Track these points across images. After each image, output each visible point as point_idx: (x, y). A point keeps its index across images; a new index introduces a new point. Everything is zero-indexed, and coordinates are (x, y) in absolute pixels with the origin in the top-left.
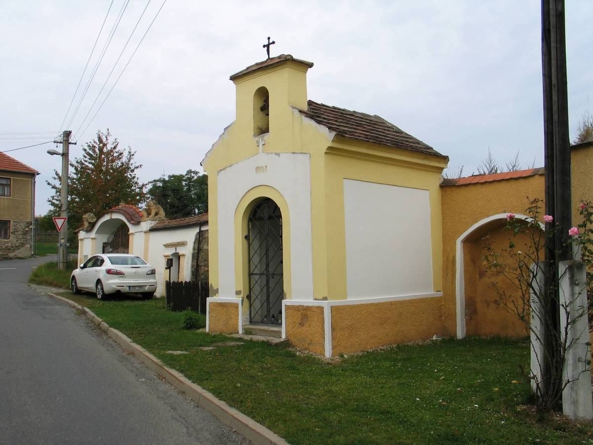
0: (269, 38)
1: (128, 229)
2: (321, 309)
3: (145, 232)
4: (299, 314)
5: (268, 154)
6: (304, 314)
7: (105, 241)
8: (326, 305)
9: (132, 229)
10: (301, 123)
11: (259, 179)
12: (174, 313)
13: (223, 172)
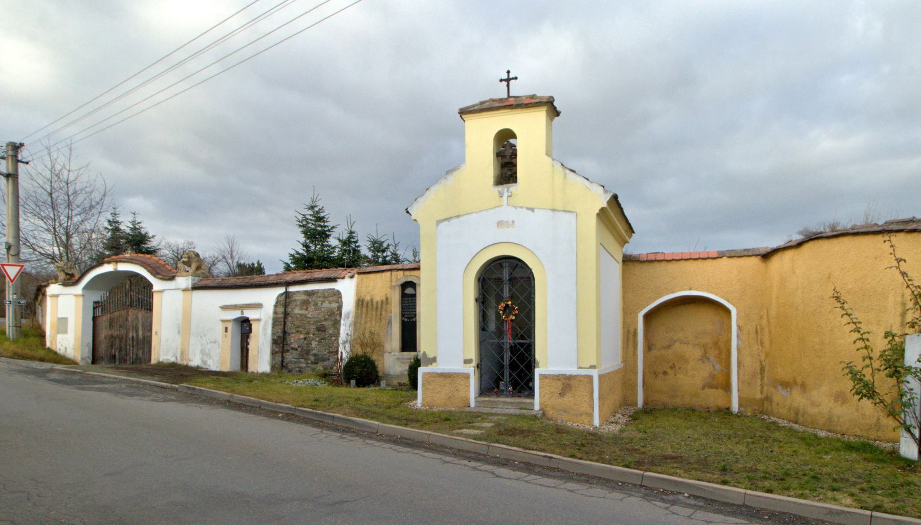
0: (508, 72)
2: (590, 378)
3: (185, 290)
4: (560, 384)
5: (515, 207)
7: (98, 299)
8: (595, 374)
9: (157, 284)
10: (565, 177)
11: (502, 235)
12: (361, 390)
13: (446, 223)
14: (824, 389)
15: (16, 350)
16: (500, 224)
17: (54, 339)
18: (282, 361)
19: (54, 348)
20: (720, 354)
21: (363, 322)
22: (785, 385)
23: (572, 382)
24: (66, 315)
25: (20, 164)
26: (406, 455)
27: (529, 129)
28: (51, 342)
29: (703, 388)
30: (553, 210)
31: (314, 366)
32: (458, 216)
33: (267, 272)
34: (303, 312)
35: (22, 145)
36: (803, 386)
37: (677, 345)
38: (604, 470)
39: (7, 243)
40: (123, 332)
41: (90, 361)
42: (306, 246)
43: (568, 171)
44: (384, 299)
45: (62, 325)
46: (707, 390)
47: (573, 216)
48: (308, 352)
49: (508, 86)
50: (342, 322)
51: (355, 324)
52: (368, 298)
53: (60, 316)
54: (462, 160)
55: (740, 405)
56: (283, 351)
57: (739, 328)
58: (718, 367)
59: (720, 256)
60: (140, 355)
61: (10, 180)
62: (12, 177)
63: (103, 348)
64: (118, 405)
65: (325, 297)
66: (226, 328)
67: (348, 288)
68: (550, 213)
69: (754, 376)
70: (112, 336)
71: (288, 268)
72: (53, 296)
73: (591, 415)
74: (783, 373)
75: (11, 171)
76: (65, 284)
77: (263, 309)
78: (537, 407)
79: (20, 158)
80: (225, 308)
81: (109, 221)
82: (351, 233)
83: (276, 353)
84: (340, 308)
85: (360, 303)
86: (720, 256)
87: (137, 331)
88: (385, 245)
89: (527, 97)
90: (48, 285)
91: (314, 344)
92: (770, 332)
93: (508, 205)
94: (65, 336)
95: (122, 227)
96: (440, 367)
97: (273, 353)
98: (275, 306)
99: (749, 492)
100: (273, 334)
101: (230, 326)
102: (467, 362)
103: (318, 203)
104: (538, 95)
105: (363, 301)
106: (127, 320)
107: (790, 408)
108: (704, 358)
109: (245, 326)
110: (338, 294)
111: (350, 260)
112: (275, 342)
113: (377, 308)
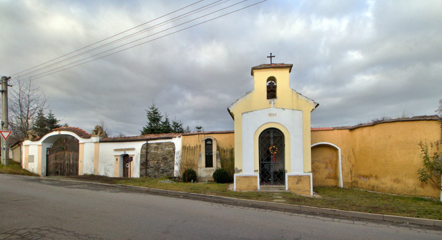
0: (271, 54)
1: (78, 141)
2: (309, 176)
3: (95, 143)
4: (296, 179)
6: (299, 179)
10: (298, 97)
11: (271, 119)
13: (246, 114)
14: (388, 177)
15: (11, 170)
16: (270, 115)
17: (27, 165)
18: (146, 173)
19: (27, 169)
20: (332, 166)
21: (186, 155)
22: (365, 177)
23: (301, 178)
24: (33, 154)
25: (8, 87)
26: (261, 212)
27: (282, 78)
28: (25, 166)
29: (326, 178)
30: (293, 110)
31: (162, 174)
32: (252, 111)
33: (109, 137)
34: (156, 152)
35: (10, 78)
36: (376, 177)
37: (316, 162)
38: (363, 215)
39: (2, 122)
40: (62, 161)
41: (45, 175)
42: (150, 124)
43: (299, 94)
44: (196, 146)
45: (31, 159)
46: (327, 179)
47: (301, 112)
48: (159, 168)
49: (271, 59)
50: (175, 156)
51: (182, 156)
52: (188, 146)
53: (30, 154)
54: (254, 89)
55: (344, 185)
56: (146, 168)
57: (342, 156)
58: (331, 171)
59: (334, 129)
60: (71, 171)
61: (4, 94)
62: (5, 92)
63: (51, 169)
64: (60, 194)
65: (166, 145)
66: (117, 159)
67: (178, 142)
68: (292, 111)
69: (348, 173)
70: (56, 163)
71: (143, 134)
72: (26, 146)
73: (310, 191)
74: (362, 172)
75: (4, 89)
76: (33, 140)
77: (135, 151)
78: (287, 189)
79: (8, 84)
80: (116, 150)
81: (38, 114)
82: (167, 119)
83: (143, 169)
84: (174, 150)
85: (184, 148)
86: (334, 129)
87: (70, 161)
88: (179, 124)
89: (280, 64)
90: (24, 141)
91: (162, 165)
92: (355, 157)
93: (273, 107)
94: (32, 163)
95: (44, 116)
96: (244, 173)
97: (141, 169)
98: (141, 149)
99: (435, 220)
100: (141, 161)
101: (119, 158)
102: (255, 171)
103: (155, 107)
104: (285, 63)
105: (185, 147)
106: (64, 156)
107: (369, 185)
108: (326, 167)
109: (126, 159)
110: (173, 144)
111: (178, 130)
112: (142, 164)
113: (192, 150)
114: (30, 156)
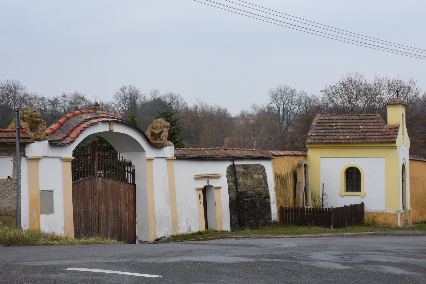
17: (35, 220)
53: (43, 187)
66: (200, 195)
94: (50, 216)
114: (43, 192)
